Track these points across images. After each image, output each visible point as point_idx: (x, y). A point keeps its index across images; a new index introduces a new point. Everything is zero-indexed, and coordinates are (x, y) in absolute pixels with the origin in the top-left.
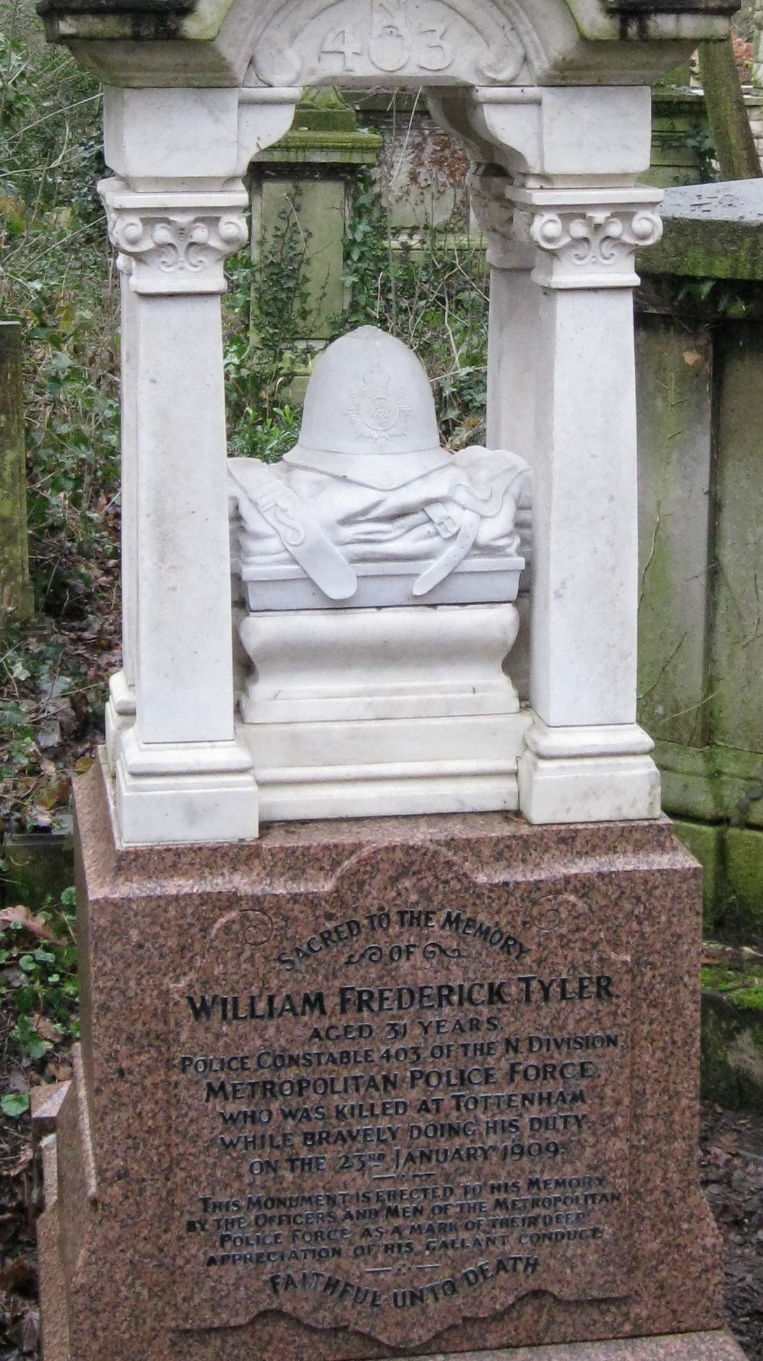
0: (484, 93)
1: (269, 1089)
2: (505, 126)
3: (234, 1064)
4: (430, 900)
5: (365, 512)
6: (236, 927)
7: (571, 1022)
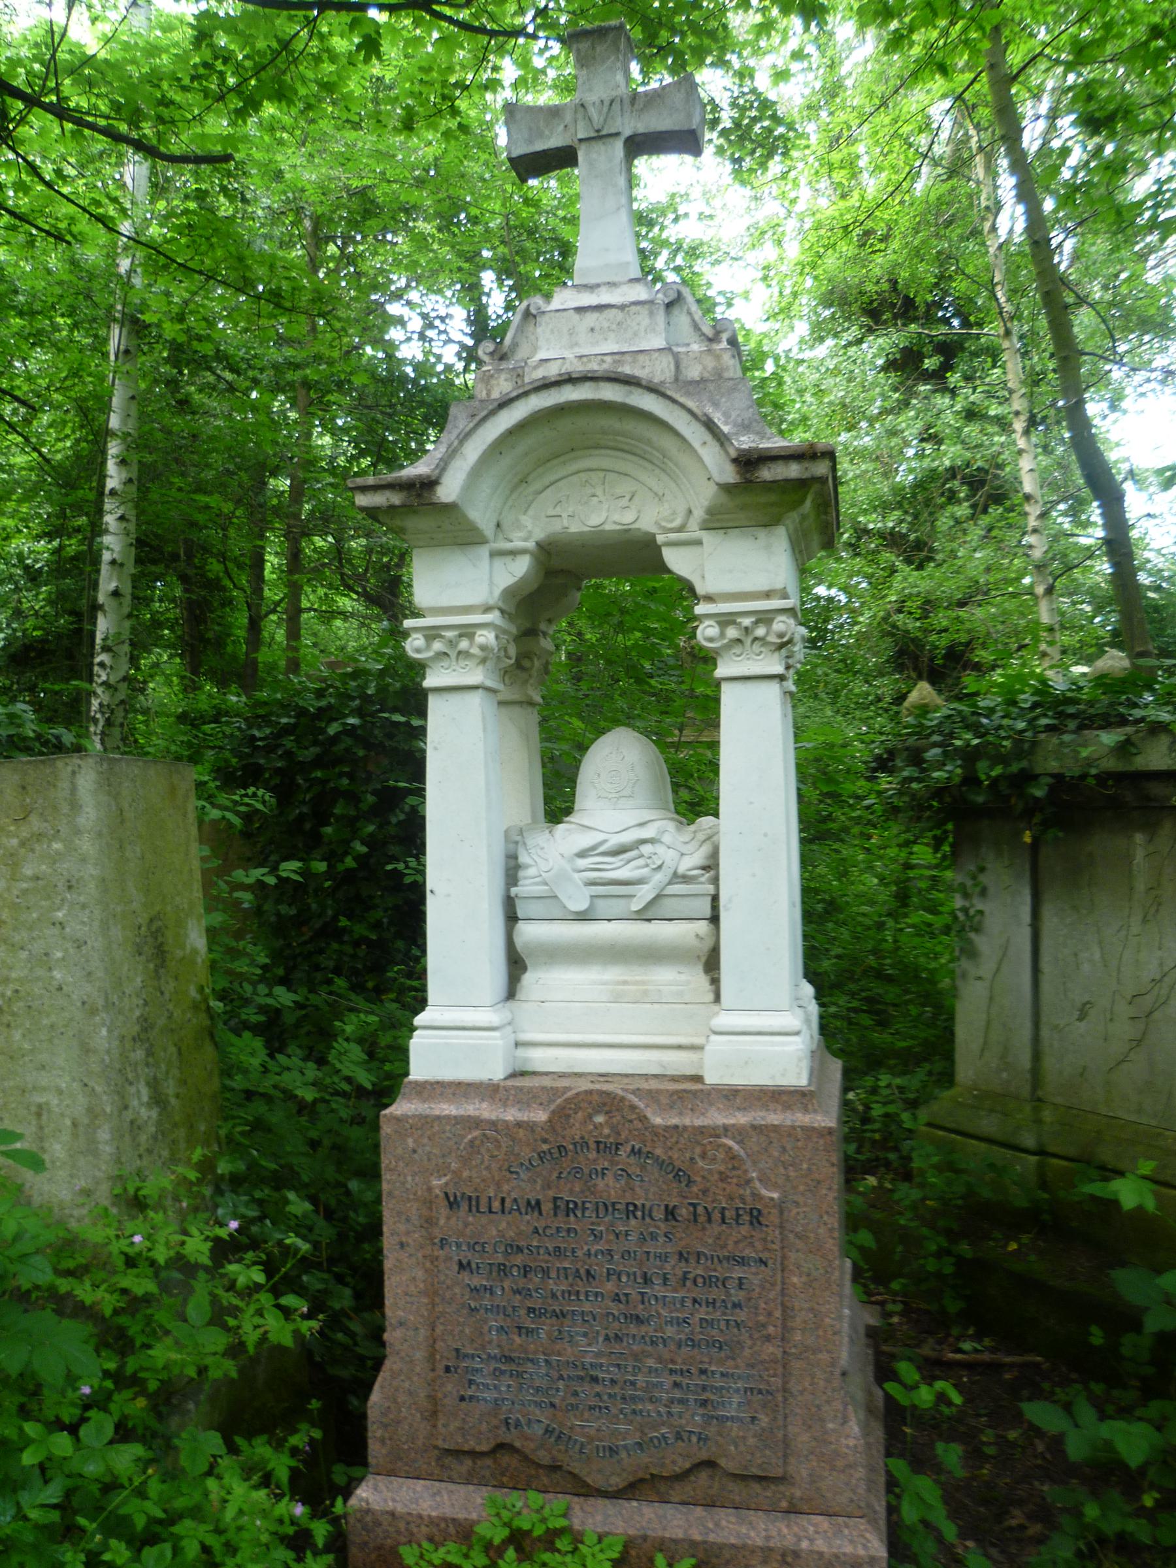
0: (660, 539)
1: (503, 1270)
2: (677, 561)
3: (477, 1248)
4: (618, 1134)
5: (593, 848)
6: (477, 1142)
7: (730, 1243)
